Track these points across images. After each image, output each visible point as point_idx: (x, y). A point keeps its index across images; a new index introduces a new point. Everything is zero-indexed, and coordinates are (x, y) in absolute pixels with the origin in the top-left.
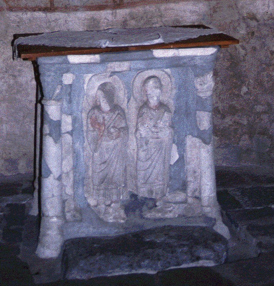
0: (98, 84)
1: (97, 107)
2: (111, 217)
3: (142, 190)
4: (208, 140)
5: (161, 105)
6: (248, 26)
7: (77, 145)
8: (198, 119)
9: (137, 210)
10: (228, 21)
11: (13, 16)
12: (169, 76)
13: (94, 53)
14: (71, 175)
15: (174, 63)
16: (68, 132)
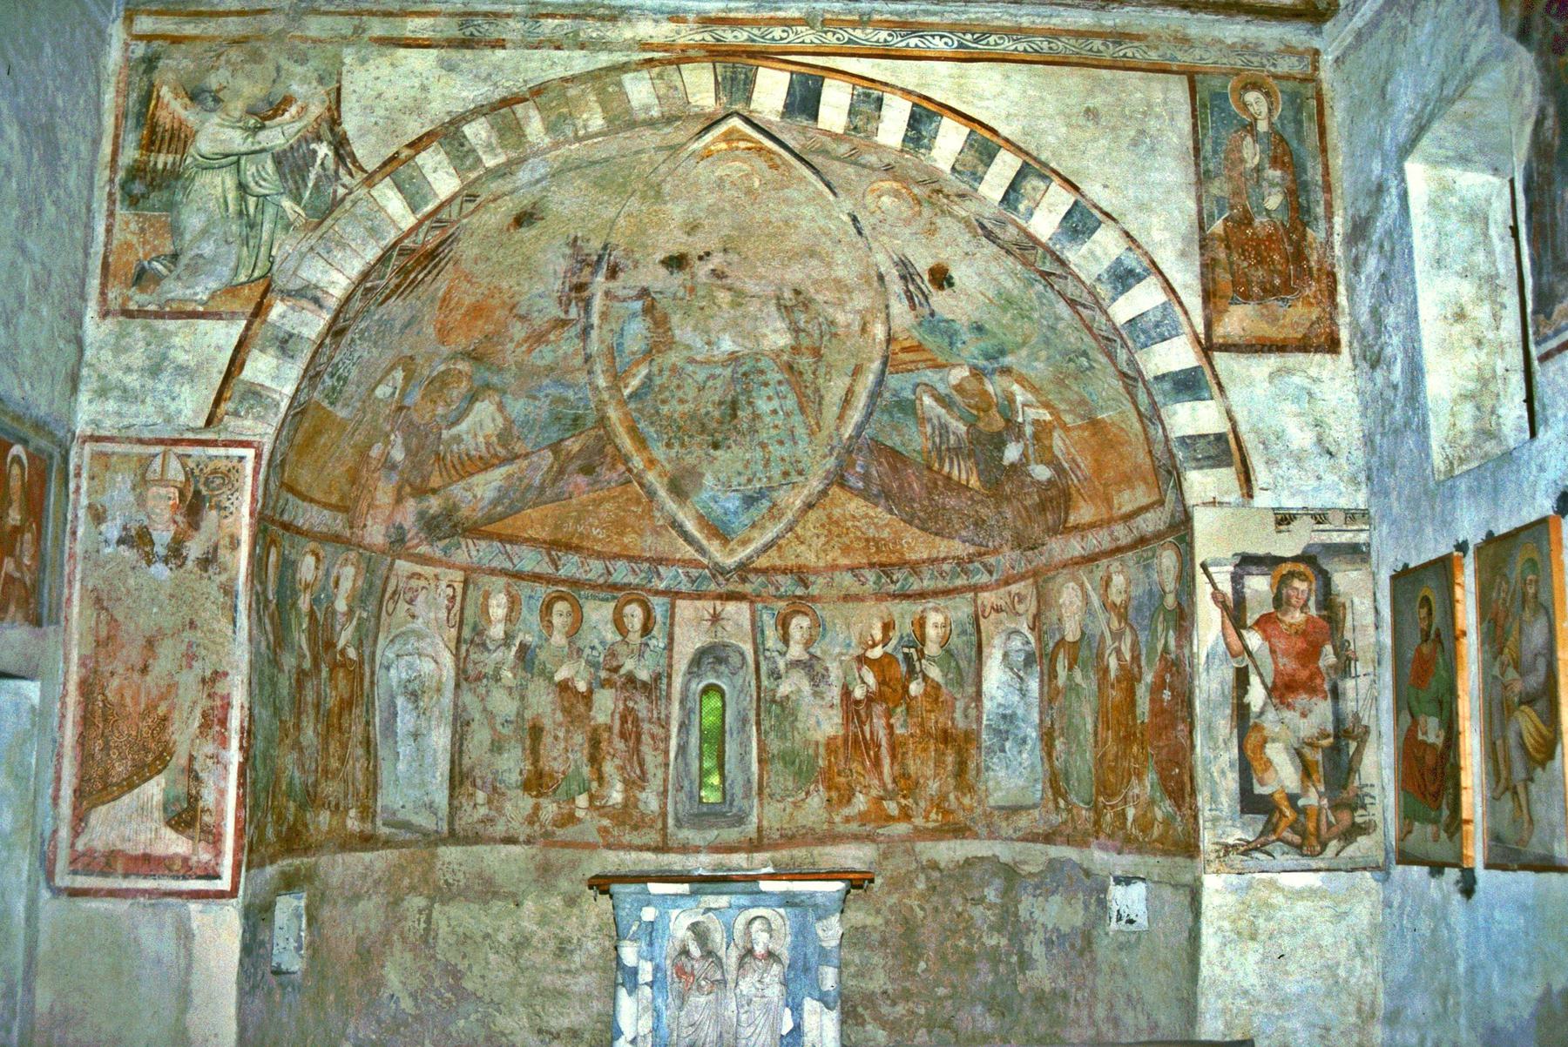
1: (685, 952)
5: (771, 955)
6: (928, 878)
7: (659, 1001)
10: (903, 871)
13: (683, 882)
14: (650, 1039)
15: (789, 901)
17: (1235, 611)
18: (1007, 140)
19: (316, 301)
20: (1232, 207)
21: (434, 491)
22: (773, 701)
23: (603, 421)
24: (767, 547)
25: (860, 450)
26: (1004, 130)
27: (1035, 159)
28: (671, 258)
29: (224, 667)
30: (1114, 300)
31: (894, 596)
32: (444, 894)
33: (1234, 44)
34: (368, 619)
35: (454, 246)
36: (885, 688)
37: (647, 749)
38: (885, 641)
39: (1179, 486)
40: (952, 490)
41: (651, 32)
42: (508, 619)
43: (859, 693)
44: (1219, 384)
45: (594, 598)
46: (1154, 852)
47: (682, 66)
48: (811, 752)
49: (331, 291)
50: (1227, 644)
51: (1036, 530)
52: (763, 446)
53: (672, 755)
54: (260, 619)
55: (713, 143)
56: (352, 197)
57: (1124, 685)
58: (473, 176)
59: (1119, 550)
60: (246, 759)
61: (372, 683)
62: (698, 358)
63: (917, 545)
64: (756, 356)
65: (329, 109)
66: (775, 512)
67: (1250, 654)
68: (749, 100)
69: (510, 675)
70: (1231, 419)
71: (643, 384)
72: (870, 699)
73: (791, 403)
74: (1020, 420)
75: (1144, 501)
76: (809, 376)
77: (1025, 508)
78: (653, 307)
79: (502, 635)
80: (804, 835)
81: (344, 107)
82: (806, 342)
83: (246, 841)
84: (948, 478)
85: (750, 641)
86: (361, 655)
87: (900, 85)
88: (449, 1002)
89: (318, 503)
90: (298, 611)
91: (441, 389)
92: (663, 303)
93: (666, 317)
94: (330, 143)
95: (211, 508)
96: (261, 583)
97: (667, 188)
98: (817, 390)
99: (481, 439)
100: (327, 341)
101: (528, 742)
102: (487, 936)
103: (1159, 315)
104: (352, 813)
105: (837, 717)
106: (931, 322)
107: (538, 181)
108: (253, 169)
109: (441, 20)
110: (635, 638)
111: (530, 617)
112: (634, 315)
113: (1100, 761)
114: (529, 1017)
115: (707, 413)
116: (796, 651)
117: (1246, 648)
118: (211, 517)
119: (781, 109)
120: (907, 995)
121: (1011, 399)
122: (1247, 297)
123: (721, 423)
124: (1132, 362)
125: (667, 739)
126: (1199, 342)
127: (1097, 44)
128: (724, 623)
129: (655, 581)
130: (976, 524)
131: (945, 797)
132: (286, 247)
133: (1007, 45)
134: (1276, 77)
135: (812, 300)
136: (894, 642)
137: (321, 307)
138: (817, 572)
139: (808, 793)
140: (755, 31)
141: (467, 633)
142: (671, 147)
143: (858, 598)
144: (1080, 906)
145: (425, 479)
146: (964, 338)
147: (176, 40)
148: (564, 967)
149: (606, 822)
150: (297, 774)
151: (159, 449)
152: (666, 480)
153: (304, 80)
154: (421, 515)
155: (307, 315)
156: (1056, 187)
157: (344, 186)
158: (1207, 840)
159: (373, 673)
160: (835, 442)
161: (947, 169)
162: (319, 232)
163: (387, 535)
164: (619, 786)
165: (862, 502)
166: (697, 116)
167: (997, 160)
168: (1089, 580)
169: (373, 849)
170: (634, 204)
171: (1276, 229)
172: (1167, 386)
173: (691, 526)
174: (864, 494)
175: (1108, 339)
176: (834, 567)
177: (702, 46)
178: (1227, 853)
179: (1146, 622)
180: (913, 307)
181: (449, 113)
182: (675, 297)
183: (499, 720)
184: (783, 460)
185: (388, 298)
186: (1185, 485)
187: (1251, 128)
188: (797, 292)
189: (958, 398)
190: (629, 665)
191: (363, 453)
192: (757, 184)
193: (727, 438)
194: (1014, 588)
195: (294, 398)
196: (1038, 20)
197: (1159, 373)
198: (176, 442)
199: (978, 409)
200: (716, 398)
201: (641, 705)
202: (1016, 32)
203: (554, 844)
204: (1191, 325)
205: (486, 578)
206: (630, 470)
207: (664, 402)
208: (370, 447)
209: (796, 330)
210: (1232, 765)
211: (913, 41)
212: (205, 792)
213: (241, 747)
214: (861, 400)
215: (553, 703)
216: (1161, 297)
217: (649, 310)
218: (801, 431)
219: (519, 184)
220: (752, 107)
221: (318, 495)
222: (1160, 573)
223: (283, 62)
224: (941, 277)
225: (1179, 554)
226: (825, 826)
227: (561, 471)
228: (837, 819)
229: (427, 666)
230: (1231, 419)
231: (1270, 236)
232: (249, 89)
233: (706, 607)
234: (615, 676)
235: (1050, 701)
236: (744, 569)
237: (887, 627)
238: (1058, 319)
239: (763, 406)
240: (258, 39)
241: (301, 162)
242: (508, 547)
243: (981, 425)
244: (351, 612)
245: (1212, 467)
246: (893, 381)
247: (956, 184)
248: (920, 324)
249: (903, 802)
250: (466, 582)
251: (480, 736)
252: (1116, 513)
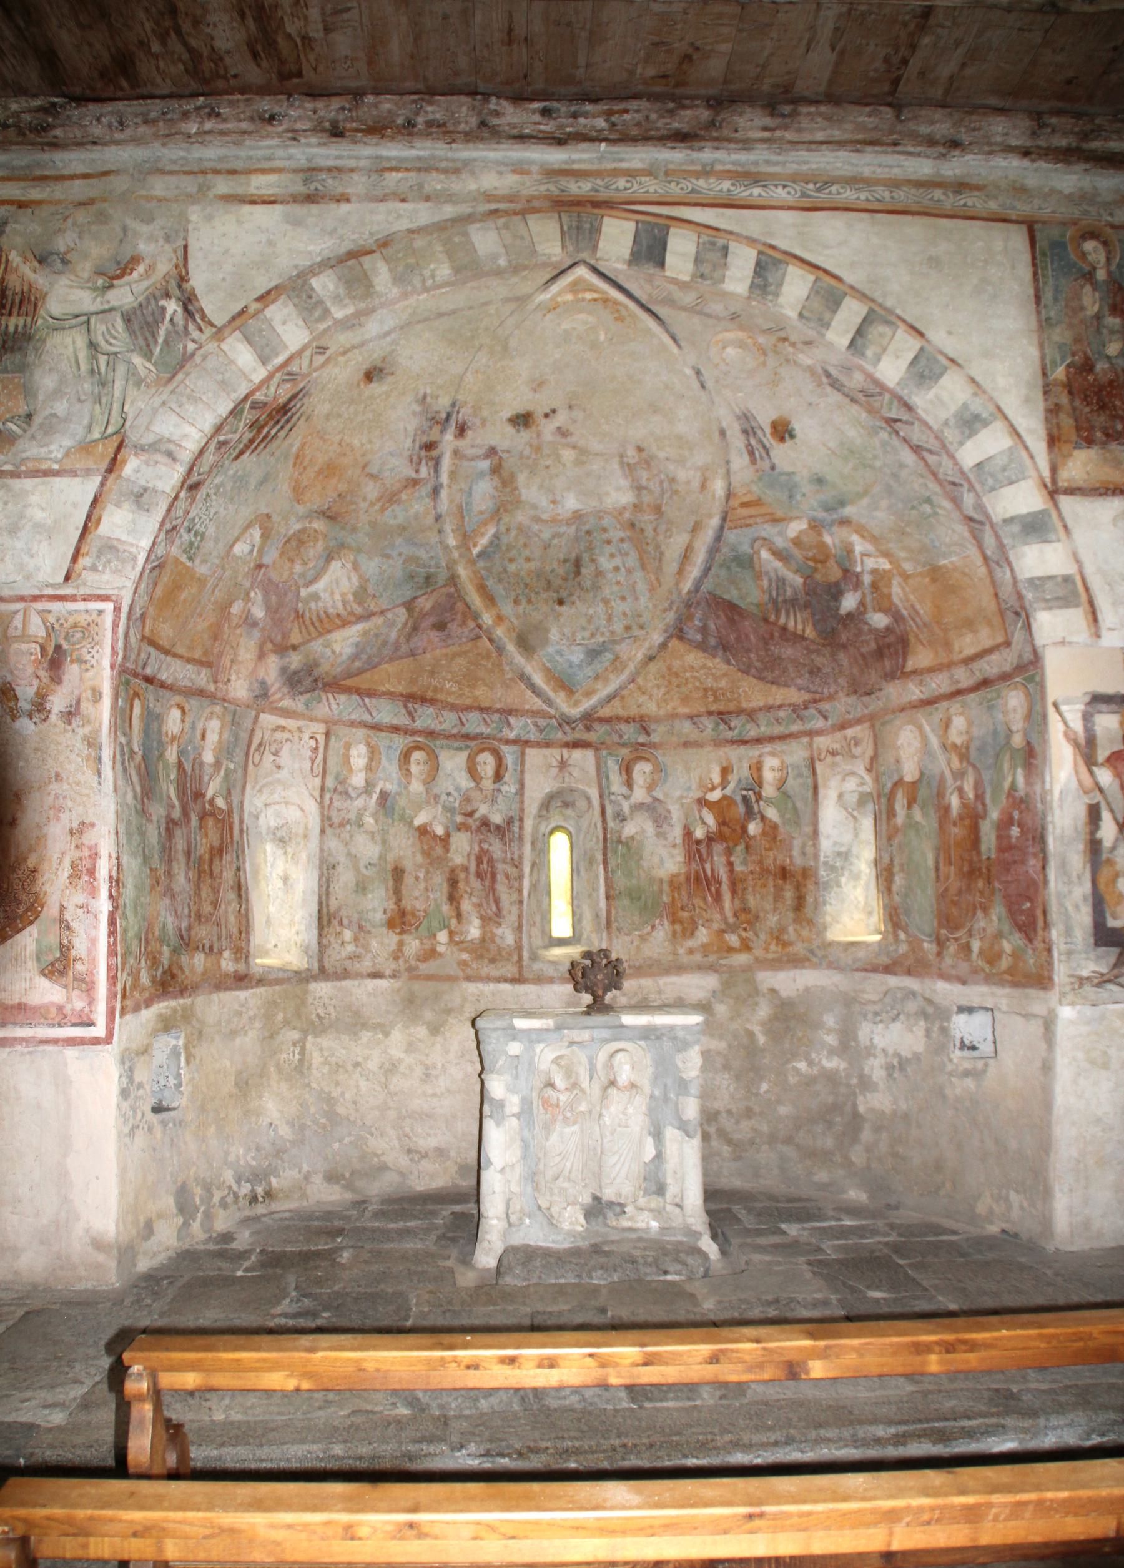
0: (552, 1056)
11: (472, 988)
15: (648, 1034)
17: (1087, 750)
18: (852, 287)
19: (170, 455)
20: (1073, 354)
21: (294, 648)
22: (619, 841)
23: (453, 579)
24: (610, 698)
25: (698, 604)
26: (849, 278)
27: (880, 305)
28: (518, 416)
29: (90, 818)
30: (961, 444)
31: (733, 742)
32: (319, 1027)
33: (1071, 194)
34: (235, 771)
35: (306, 400)
36: (725, 829)
37: (501, 888)
38: (724, 784)
39: (1028, 626)
40: (787, 640)
41: (497, 184)
42: (369, 768)
43: (699, 833)
44: (1065, 527)
45: (449, 747)
46: (1001, 983)
47: (528, 216)
48: (655, 888)
49: (184, 444)
50: (1079, 781)
51: (873, 676)
52: (606, 602)
53: (525, 893)
54: (125, 770)
55: (559, 294)
56: (201, 352)
57: (967, 822)
58: (322, 326)
59: (959, 692)
60: (116, 908)
61: (241, 831)
62: (545, 517)
63: (753, 693)
64: (599, 514)
65: (177, 267)
66: (617, 663)
67: (1101, 790)
68: (595, 248)
69: (372, 821)
70: (1078, 561)
71: (491, 543)
72: (710, 839)
73: (632, 560)
74: (859, 569)
75: (988, 643)
76: (649, 533)
77: (863, 656)
78: (500, 465)
79: (363, 784)
80: (650, 966)
81: (191, 264)
82: (647, 498)
83: (119, 988)
84: (784, 629)
85: (595, 785)
86: (229, 804)
87: (745, 233)
88: (324, 1127)
89: (181, 657)
90: (166, 766)
91: (298, 547)
92: (510, 462)
93: (512, 476)
94: (179, 299)
95: (72, 661)
96: (125, 734)
97: (513, 343)
98: (657, 547)
99: (337, 597)
100: (183, 495)
101: (391, 883)
102: (357, 1065)
103: (1006, 460)
104: (226, 954)
105: (679, 856)
106: (772, 476)
107: (387, 334)
108: (103, 328)
109: (283, 177)
110: (488, 784)
111: (390, 767)
112: (481, 475)
113: (942, 896)
114: (399, 1139)
115: (552, 571)
116: (639, 794)
117: (1097, 784)
118: (72, 671)
119: (627, 256)
120: (749, 1113)
121: (849, 551)
122: (1090, 442)
123: (565, 579)
124: (980, 506)
125: (521, 877)
126: (1045, 486)
127: (938, 194)
128: (570, 769)
129: (506, 731)
130: (811, 672)
131: (782, 930)
132: (138, 403)
133: (848, 195)
134: (1113, 226)
135: (652, 457)
136: (732, 785)
137: (174, 459)
138: (658, 720)
139: (653, 927)
140: (599, 182)
141: (330, 782)
142: (517, 299)
143: (697, 745)
144: (921, 1033)
145: (285, 636)
146: (804, 490)
147: (21, 205)
148: (430, 1092)
149: (465, 956)
150: (170, 920)
151: (19, 606)
152: (514, 635)
153: (151, 238)
154: (284, 670)
155: (162, 469)
156: (901, 333)
157: (194, 341)
158: (1061, 972)
159: (241, 822)
160: (674, 597)
161: (793, 314)
162: (170, 387)
163: (250, 690)
164: (477, 922)
165: (700, 654)
166: (544, 265)
167: (843, 306)
168: (928, 722)
169: (247, 988)
170: (482, 358)
171: (1117, 375)
172: (1016, 528)
173: (538, 679)
174: (702, 646)
175: (954, 484)
176: (673, 716)
177: (547, 197)
178: (1081, 985)
179: (991, 761)
180: (753, 461)
181: (296, 266)
182: (521, 456)
183: (362, 864)
184: (625, 614)
185: (241, 453)
186: (1034, 627)
187: (1089, 276)
188: (640, 449)
189: (796, 552)
190: (483, 810)
191: (224, 608)
192: (602, 337)
193: (571, 595)
194: (850, 732)
195: (150, 551)
196: (879, 170)
197: (1008, 515)
198: (36, 598)
199: (816, 561)
200: (562, 556)
201: (496, 848)
202: (854, 181)
203: (418, 978)
204: (1037, 470)
205: (347, 730)
206: (480, 627)
207: (511, 560)
208: (230, 604)
209: (639, 489)
210: (1085, 899)
211: (756, 191)
212: (76, 942)
213: (111, 896)
214: (700, 557)
215: (413, 846)
216: (1006, 442)
217: (496, 470)
218: (641, 587)
219: (367, 336)
220: (599, 254)
221: (180, 650)
222: (1005, 713)
223: (128, 221)
224: (782, 431)
225: (1028, 694)
226: (670, 958)
227: (415, 629)
228: (681, 951)
229: (293, 814)
230: (1078, 561)
231: (1111, 382)
232: (97, 250)
233: (554, 755)
234: (470, 821)
235: (890, 838)
236: (589, 719)
237: (725, 771)
238: (902, 466)
239: (605, 563)
240: (104, 200)
241: (150, 319)
242: (367, 700)
243: (818, 577)
244: (217, 764)
245: (1060, 608)
246: (731, 536)
247: (800, 331)
248: (760, 479)
249: (744, 934)
250: (327, 734)
251: (345, 878)
252: (956, 657)
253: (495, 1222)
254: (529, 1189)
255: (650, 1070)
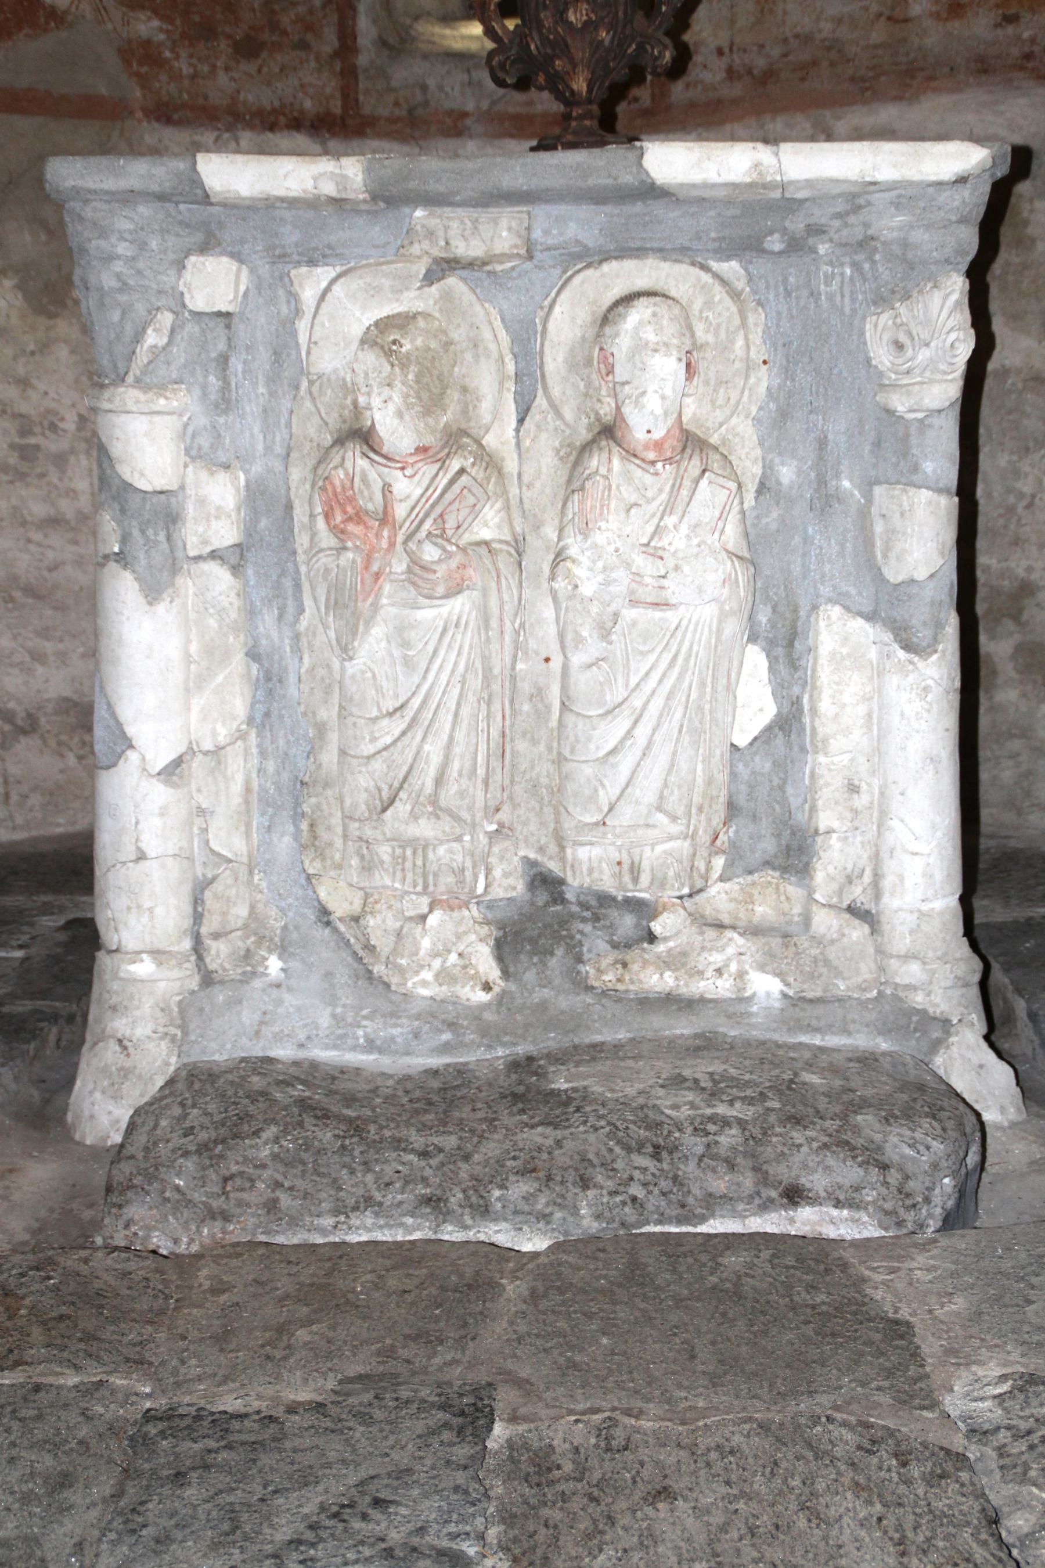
2: (427, 975)
3: (583, 853)
4: (922, 635)
8: (879, 528)
9: (560, 952)
12: (735, 295)
16: (214, 555)
80: (805, 70)
148: (39, 510)
226: (878, 34)
253: (144, 968)
254: (284, 844)
255: (762, 381)
